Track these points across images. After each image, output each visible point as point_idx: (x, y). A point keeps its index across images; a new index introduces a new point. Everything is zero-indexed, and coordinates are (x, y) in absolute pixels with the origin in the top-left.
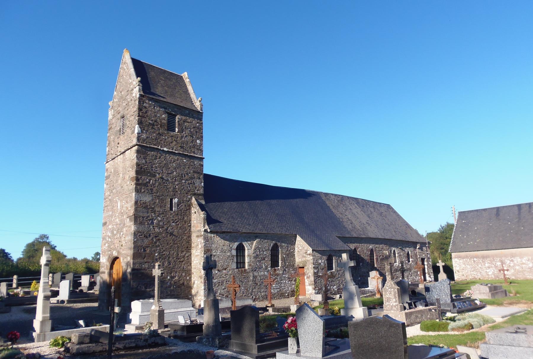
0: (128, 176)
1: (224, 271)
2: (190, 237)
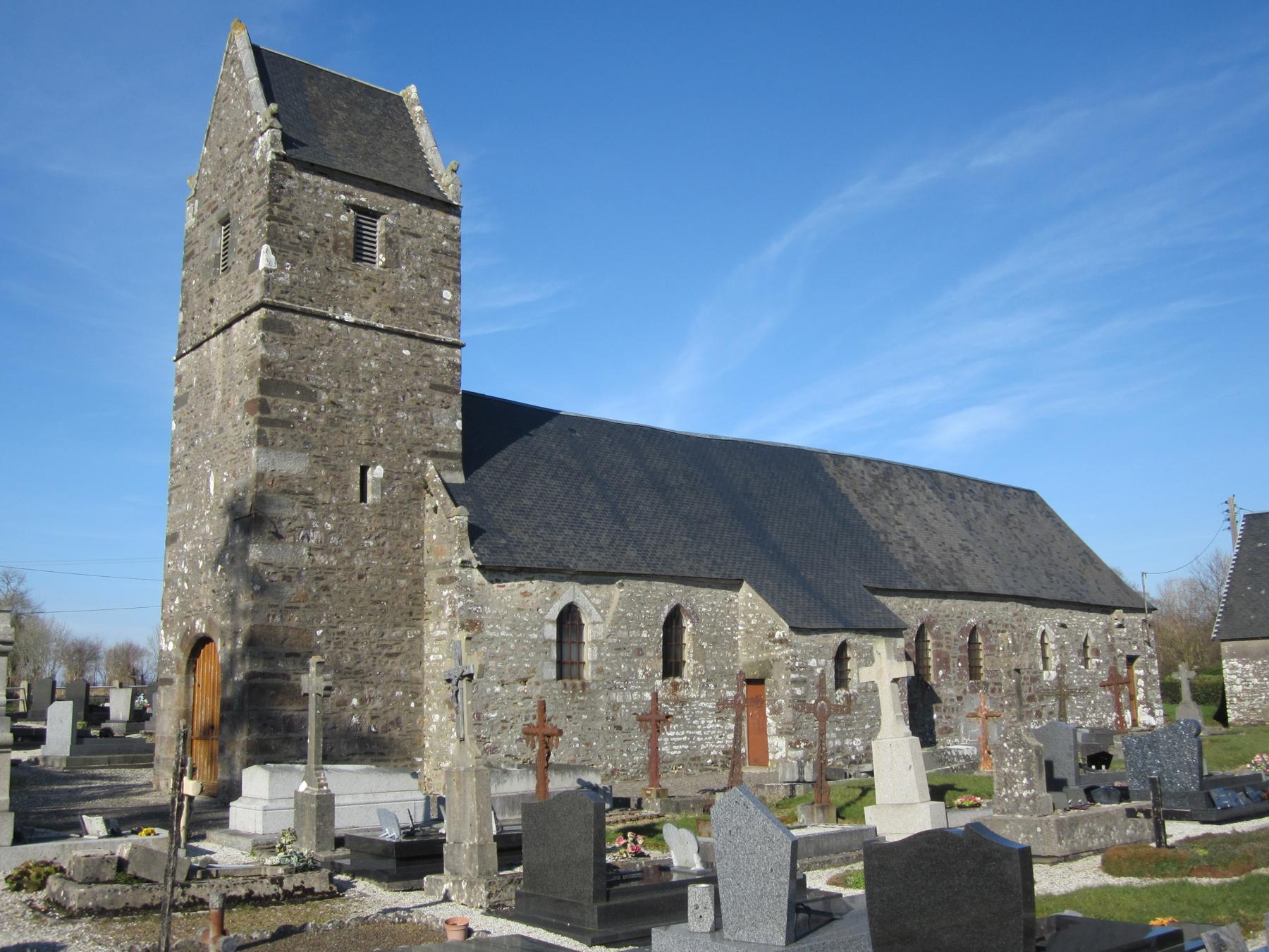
0: (237, 398)
1: (520, 688)
2: (418, 582)
